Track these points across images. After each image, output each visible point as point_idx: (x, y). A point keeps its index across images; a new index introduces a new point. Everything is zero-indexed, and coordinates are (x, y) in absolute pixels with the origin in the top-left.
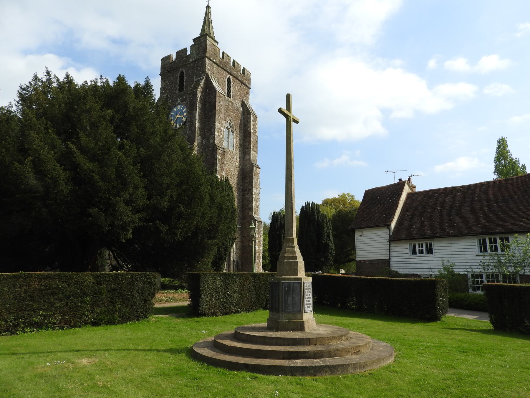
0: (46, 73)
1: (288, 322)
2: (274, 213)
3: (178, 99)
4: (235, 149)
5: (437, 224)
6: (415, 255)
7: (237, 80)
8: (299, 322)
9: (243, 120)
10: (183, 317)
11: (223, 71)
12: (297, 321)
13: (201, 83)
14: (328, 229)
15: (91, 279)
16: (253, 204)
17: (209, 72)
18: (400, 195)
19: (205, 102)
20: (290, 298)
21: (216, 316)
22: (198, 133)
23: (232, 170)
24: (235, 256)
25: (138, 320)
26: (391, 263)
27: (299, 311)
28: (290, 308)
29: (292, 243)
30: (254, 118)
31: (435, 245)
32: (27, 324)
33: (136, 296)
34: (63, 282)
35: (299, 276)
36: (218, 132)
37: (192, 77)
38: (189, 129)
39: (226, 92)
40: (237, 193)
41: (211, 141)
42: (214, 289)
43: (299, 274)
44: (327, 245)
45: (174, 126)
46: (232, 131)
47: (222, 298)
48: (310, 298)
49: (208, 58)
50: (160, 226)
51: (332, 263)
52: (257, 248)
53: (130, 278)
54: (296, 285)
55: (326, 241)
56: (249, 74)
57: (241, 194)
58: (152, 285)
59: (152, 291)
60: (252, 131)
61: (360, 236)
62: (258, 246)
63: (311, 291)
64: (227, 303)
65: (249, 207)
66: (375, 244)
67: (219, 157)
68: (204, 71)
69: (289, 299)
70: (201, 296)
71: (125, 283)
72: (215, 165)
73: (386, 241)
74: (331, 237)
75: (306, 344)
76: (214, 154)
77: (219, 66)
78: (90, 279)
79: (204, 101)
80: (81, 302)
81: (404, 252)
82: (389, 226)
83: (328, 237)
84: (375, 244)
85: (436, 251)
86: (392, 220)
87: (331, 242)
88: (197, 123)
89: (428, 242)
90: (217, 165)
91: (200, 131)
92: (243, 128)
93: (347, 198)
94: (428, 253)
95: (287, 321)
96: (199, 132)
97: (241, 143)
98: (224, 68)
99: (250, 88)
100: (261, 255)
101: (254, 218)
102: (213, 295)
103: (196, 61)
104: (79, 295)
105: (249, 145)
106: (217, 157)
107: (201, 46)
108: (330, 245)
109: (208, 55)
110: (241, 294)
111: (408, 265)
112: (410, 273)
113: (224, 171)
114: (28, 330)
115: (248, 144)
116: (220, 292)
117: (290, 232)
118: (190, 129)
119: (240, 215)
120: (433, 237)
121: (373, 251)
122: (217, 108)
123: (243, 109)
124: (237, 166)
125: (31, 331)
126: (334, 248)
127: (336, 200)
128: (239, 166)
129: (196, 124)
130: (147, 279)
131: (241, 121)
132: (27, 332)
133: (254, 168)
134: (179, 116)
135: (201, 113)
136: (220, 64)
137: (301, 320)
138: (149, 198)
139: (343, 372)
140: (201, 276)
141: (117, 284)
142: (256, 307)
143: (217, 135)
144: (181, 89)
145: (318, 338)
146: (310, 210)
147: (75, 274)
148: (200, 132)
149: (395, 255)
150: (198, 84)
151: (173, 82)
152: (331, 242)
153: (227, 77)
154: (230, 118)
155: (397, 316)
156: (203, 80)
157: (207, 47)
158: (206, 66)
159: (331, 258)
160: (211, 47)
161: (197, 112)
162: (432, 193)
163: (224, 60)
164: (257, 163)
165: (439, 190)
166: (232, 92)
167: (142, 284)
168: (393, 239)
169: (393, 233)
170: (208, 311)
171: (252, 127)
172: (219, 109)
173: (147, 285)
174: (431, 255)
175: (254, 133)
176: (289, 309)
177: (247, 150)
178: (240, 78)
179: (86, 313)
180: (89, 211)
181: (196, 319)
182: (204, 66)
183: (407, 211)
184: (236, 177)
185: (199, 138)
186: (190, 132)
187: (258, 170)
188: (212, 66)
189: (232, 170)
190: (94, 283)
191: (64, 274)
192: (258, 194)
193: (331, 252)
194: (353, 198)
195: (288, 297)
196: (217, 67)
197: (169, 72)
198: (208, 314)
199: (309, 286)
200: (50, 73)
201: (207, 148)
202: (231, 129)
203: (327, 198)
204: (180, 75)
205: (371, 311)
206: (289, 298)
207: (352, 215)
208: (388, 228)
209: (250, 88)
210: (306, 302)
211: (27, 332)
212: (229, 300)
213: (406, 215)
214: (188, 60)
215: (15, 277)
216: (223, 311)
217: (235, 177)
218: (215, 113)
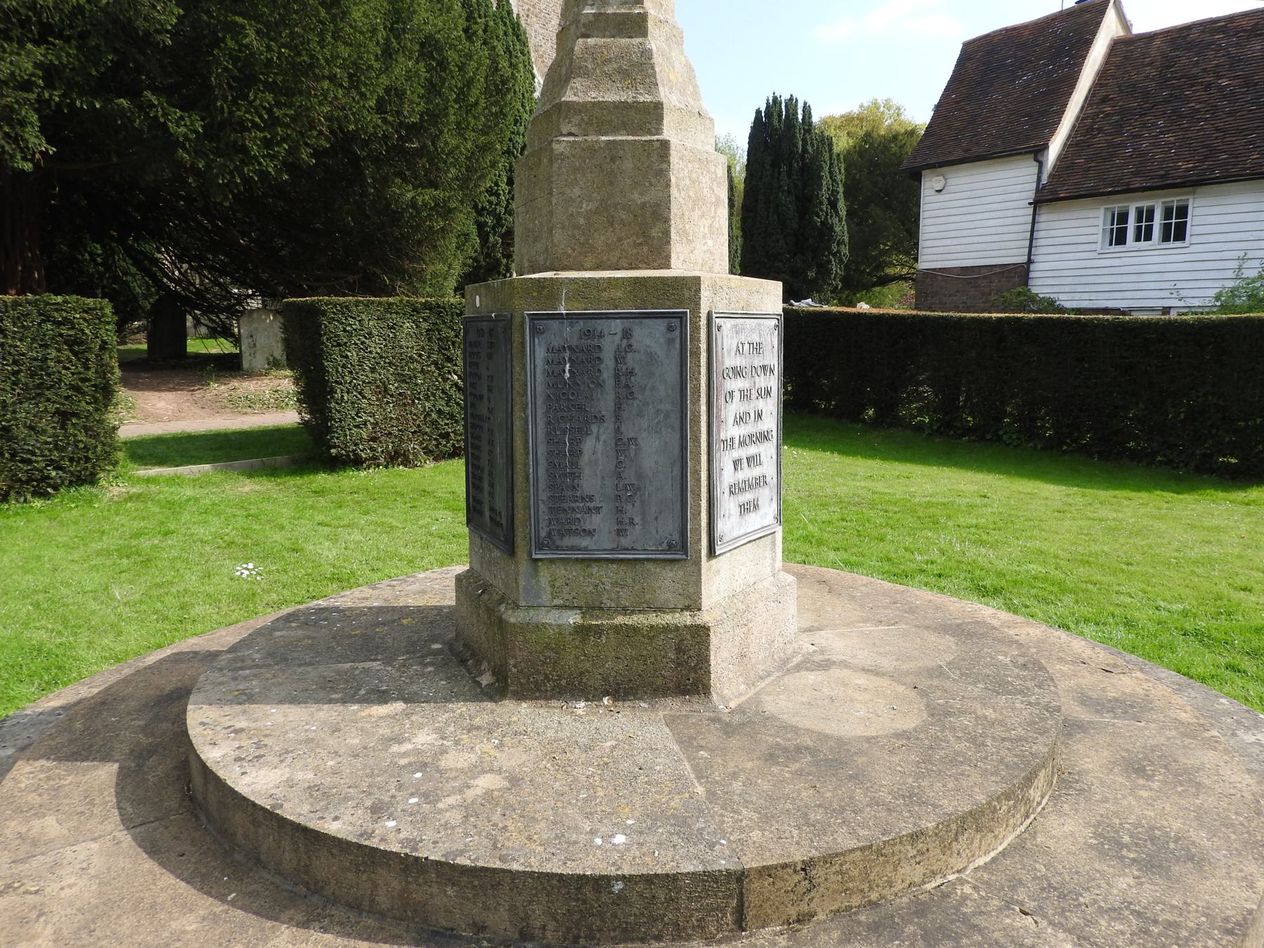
1: (582, 631)
5: (1217, 138)
6: (1120, 248)
8: (666, 629)
10: (272, 472)
12: (654, 619)
14: (833, 182)
18: (1087, 44)
21: (406, 462)
26: (1032, 275)
28: (595, 521)
31: (1197, 211)
35: (678, 269)
42: (390, 363)
43: (673, 262)
44: (827, 229)
47: (427, 399)
48: (764, 437)
50: (165, 115)
51: (837, 285)
55: (826, 218)
58: (89, 350)
61: (939, 191)
63: (773, 382)
64: (452, 417)
66: (986, 215)
69: (585, 458)
70: (333, 391)
73: (1025, 203)
74: (842, 205)
75: (701, 927)
81: (1083, 239)
82: (1038, 152)
83: (833, 204)
84: (986, 215)
85: (1196, 230)
86: (1052, 132)
87: (840, 220)
89: (1175, 201)
93: (883, 113)
94: (1166, 238)
95: (573, 618)
102: (386, 390)
108: (837, 229)
111: (1091, 280)
112: (1095, 306)
116: (416, 377)
120: (1197, 182)
121: (976, 239)
126: (846, 239)
127: (853, 118)
137: (686, 619)
140: (324, 313)
145: (828, 859)
146: (780, 120)
149: (1050, 250)
152: (840, 220)
155: (1096, 456)
159: (836, 269)
162: (1203, 32)
165: (1231, 19)
168: (1045, 198)
169: (1051, 176)
170: (372, 449)
173: (59, 350)
174: (1178, 244)
176: (590, 533)
181: (322, 479)
183: (1105, 100)
193: (838, 251)
194: (898, 115)
195: (576, 442)
198: (375, 458)
199: (757, 348)
203: (828, 115)
205: (988, 437)
206: (588, 445)
207: (902, 147)
208: (1036, 160)
210: (727, 476)
213: (1103, 112)
216: (437, 446)
217: (553, 23)
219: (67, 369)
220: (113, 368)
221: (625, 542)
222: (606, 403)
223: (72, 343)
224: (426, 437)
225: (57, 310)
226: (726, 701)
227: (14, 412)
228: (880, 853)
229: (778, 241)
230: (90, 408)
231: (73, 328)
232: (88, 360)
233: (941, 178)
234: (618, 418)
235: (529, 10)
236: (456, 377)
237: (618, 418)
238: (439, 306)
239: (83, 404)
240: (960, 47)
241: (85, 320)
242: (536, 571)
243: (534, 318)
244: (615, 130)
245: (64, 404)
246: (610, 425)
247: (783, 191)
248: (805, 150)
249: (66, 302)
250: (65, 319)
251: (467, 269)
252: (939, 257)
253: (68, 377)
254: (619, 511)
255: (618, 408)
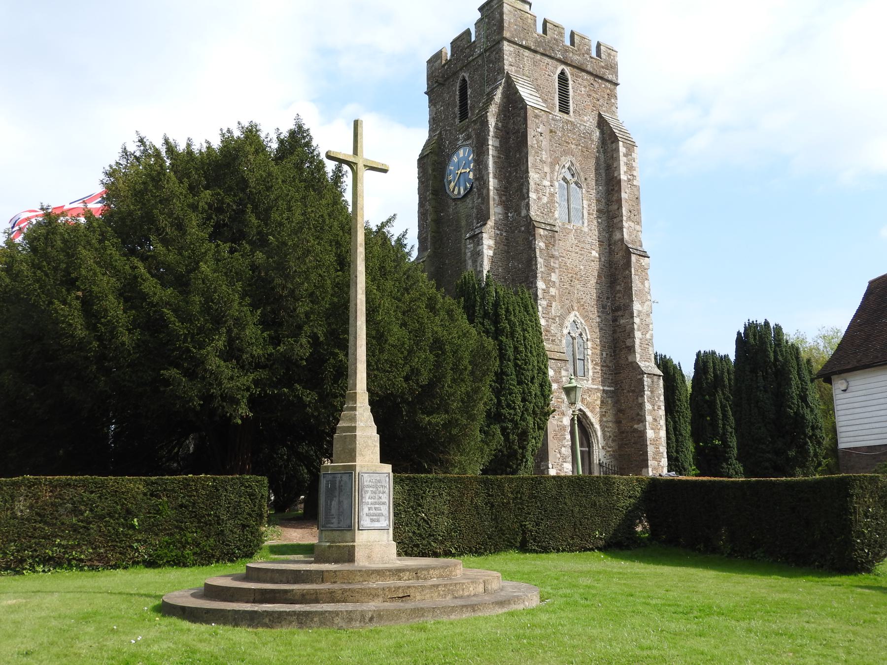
0: (139, 141)
1: (329, 547)
2: (698, 354)
3: (460, 136)
4: (586, 222)
7: (583, 74)
8: (346, 546)
9: (602, 156)
11: (547, 60)
12: (345, 544)
13: (495, 95)
15: (141, 487)
16: (634, 337)
17: (513, 68)
19: (508, 133)
20: (334, 503)
22: (494, 199)
23: (582, 267)
24: (602, 453)
25: (232, 561)
27: (349, 527)
29: (353, 401)
30: (627, 148)
32: (37, 559)
33: (225, 517)
34: (92, 492)
36: (537, 191)
37: (480, 87)
38: (479, 195)
39: (558, 104)
40: (599, 316)
41: (523, 213)
45: (456, 192)
46: (576, 183)
49: (509, 41)
52: (650, 434)
53: (213, 486)
54: (345, 478)
55: (798, 409)
56: (613, 53)
57: (610, 317)
58: (256, 498)
59: (256, 508)
60: (623, 177)
61: (844, 391)
62: (652, 429)
64: (421, 535)
65: (628, 344)
66: (877, 408)
67: (540, 244)
68: (501, 70)
71: (202, 494)
72: (534, 263)
75: (316, 581)
76: (531, 239)
77: (535, 52)
78: (138, 488)
79: (504, 133)
80: (123, 526)
84: (877, 408)
88: (491, 180)
90: (536, 262)
91: (500, 196)
92: (604, 175)
96: (496, 197)
97: (602, 208)
98: (547, 53)
99: (617, 84)
100: (663, 449)
101: (639, 367)
103: (486, 51)
104: (120, 513)
105: (618, 209)
106: (535, 244)
107: (493, 20)
109: (506, 34)
110: (454, 519)
113: (554, 272)
114: (40, 569)
115: (616, 207)
117: (351, 382)
118: (480, 195)
119: (610, 365)
122: (531, 141)
123: (602, 132)
124: (595, 257)
125: (44, 571)
128: (600, 258)
129: (489, 181)
130: (246, 487)
131: (597, 159)
132: (38, 572)
133: (634, 258)
134: (463, 171)
135: (499, 157)
136: (539, 46)
137: (352, 544)
138: (276, 341)
139: (322, 623)
141: (188, 496)
142: (497, 545)
143: (535, 197)
144: (464, 115)
146: (755, 339)
147: (111, 480)
148: (500, 197)
150: (490, 99)
151: (449, 105)
153: (559, 72)
154: (569, 158)
156: (501, 88)
157: (505, 17)
158: (505, 57)
160: (515, 15)
161: (490, 157)
163: (548, 37)
164: (641, 246)
166: (571, 102)
167: (235, 498)
171: (623, 168)
172: (535, 142)
173: (245, 498)
175: (629, 180)
176: (333, 523)
177: (615, 221)
178: (589, 68)
179: (135, 545)
180: (163, 374)
182: (500, 59)
184: (593, 281)
185: (499, 210)
186: (480, 199)
187: (644, 261)
188: (518, 55)
189: (582, 267)
190: (145, 494)
191: (92, 479)
192: (648, 315)
195: (331, 502)
196: (531, 55)
197: (440, 84)
200: (145, 140)
201: (516, 229)
202: (573, 180)
204: (460, 87)
206: (333, 503)
209: (617, 84)
211: (38, 572)
212: (424, 529)
214: (472, 53)
215: (14, 484)
217: (591, 282)
218: (527, 153)
219: (247, 506)
220: (264, 506)
221: (340, 525)
222: (337, 494)
223: (251, 495)
224: (406, 546)
225: (247, 481)
226: (358, 564)
227: (226, 524)
228: (351, 572)
229: (760, 428)
230: (254, 523)
231: (252, 489)
232: (255, 502)
233: (843, 381)
234: (339, 496)
235: (572, 277)
236: (423, 515)
237: (339, 496)
238: (414, 478)
239: (252, 521)
240: (867, 284)
241: (256, 485)
242: (322, 533)
243: (324, 474)
244: (347, 432)
245: (244, 521)
246: (337, 498)
247: (761, 391)
248: (776, 359)
249: (250, 478)
250: (249, 485)
251: (492, 457)
252: (852, 439)
253: (247, 510)
254: (339, 518)
255: (339, 494)
